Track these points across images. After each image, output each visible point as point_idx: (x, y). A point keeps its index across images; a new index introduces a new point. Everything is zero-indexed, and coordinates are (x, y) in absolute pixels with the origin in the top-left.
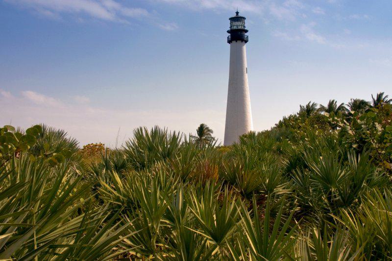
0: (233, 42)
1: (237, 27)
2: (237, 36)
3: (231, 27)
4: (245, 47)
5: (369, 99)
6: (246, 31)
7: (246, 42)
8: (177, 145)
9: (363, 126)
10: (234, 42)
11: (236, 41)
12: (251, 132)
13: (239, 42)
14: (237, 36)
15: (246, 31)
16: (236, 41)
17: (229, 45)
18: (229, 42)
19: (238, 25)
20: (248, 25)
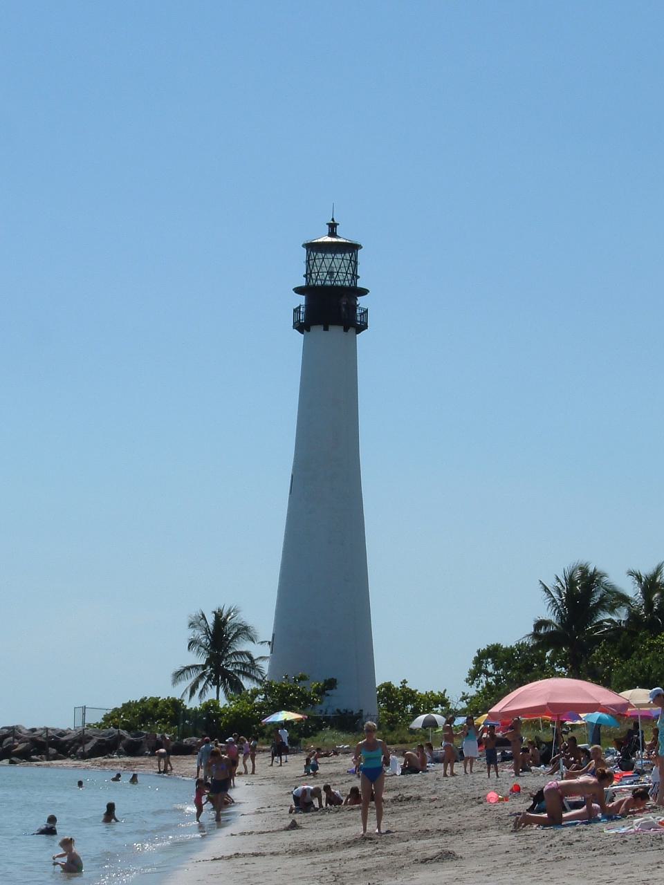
0: (313, 328)
1: (268, 741)
2: (331, 308)
3: (308, 275)
4: (361, 337)
5: (397, 684)
6: (364, 292)
7: (362, 327)
8: (538, 643)
9: (440, 711)
10: (317, 330)
11: (326, 329)
12: (338, 710)
13: (336, 331)
14: (331, 308)
15: (364, 292)
16: (326, 329)
17: (299, 337)
18: (301, 327)
19: (333, 269)
20: (370, 272)
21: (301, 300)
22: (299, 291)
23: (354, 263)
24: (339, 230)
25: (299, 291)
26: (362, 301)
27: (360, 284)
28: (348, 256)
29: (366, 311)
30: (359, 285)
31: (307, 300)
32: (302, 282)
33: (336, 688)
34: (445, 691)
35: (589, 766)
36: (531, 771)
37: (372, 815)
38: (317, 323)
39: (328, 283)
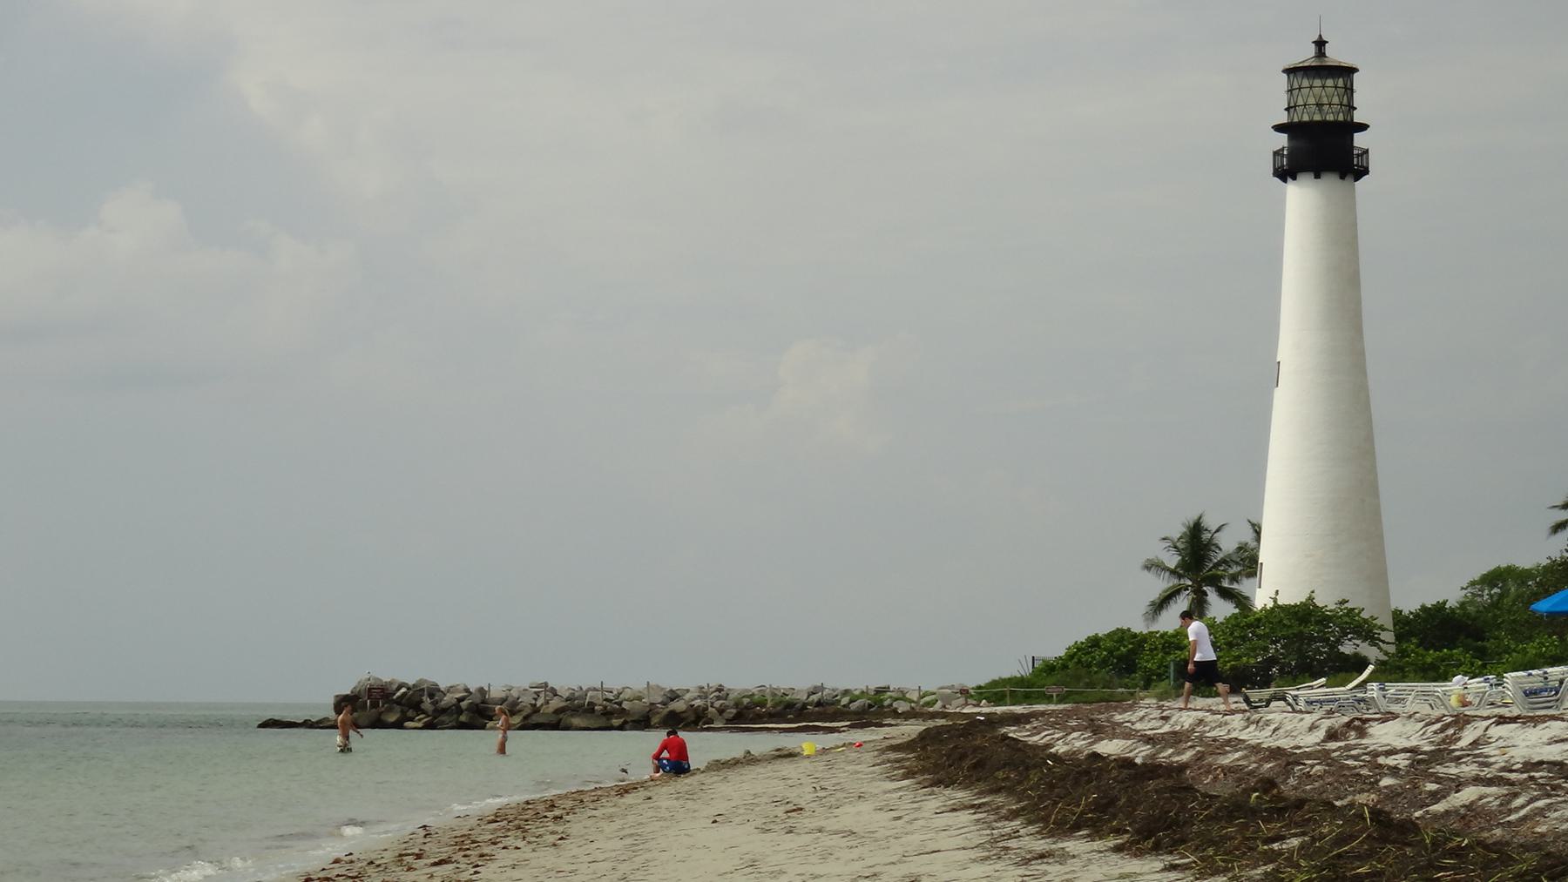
6: (1363, 127)
7: (1364, 171)
13: (1330, 182)
15: (1363, 127)
19: (1318, 102)
21: (1282, 140)
22: (1279, 128)
23: (1349, 90)
24: (1328, 50)
25: (1279, 128)
26: (1360, 140)
27: (1358, 117)
28: (1341, 82)
29: (1366, 152)
30: (1356, 120)
31: (1290, 139)
32: (1283, 118)
33: (1311, 599)
34: (1320, 44)
35: (1017, 720)
36: (341, 836)
37: (1182, 603)
38: (1305, 169)
39: (1317, 118)
